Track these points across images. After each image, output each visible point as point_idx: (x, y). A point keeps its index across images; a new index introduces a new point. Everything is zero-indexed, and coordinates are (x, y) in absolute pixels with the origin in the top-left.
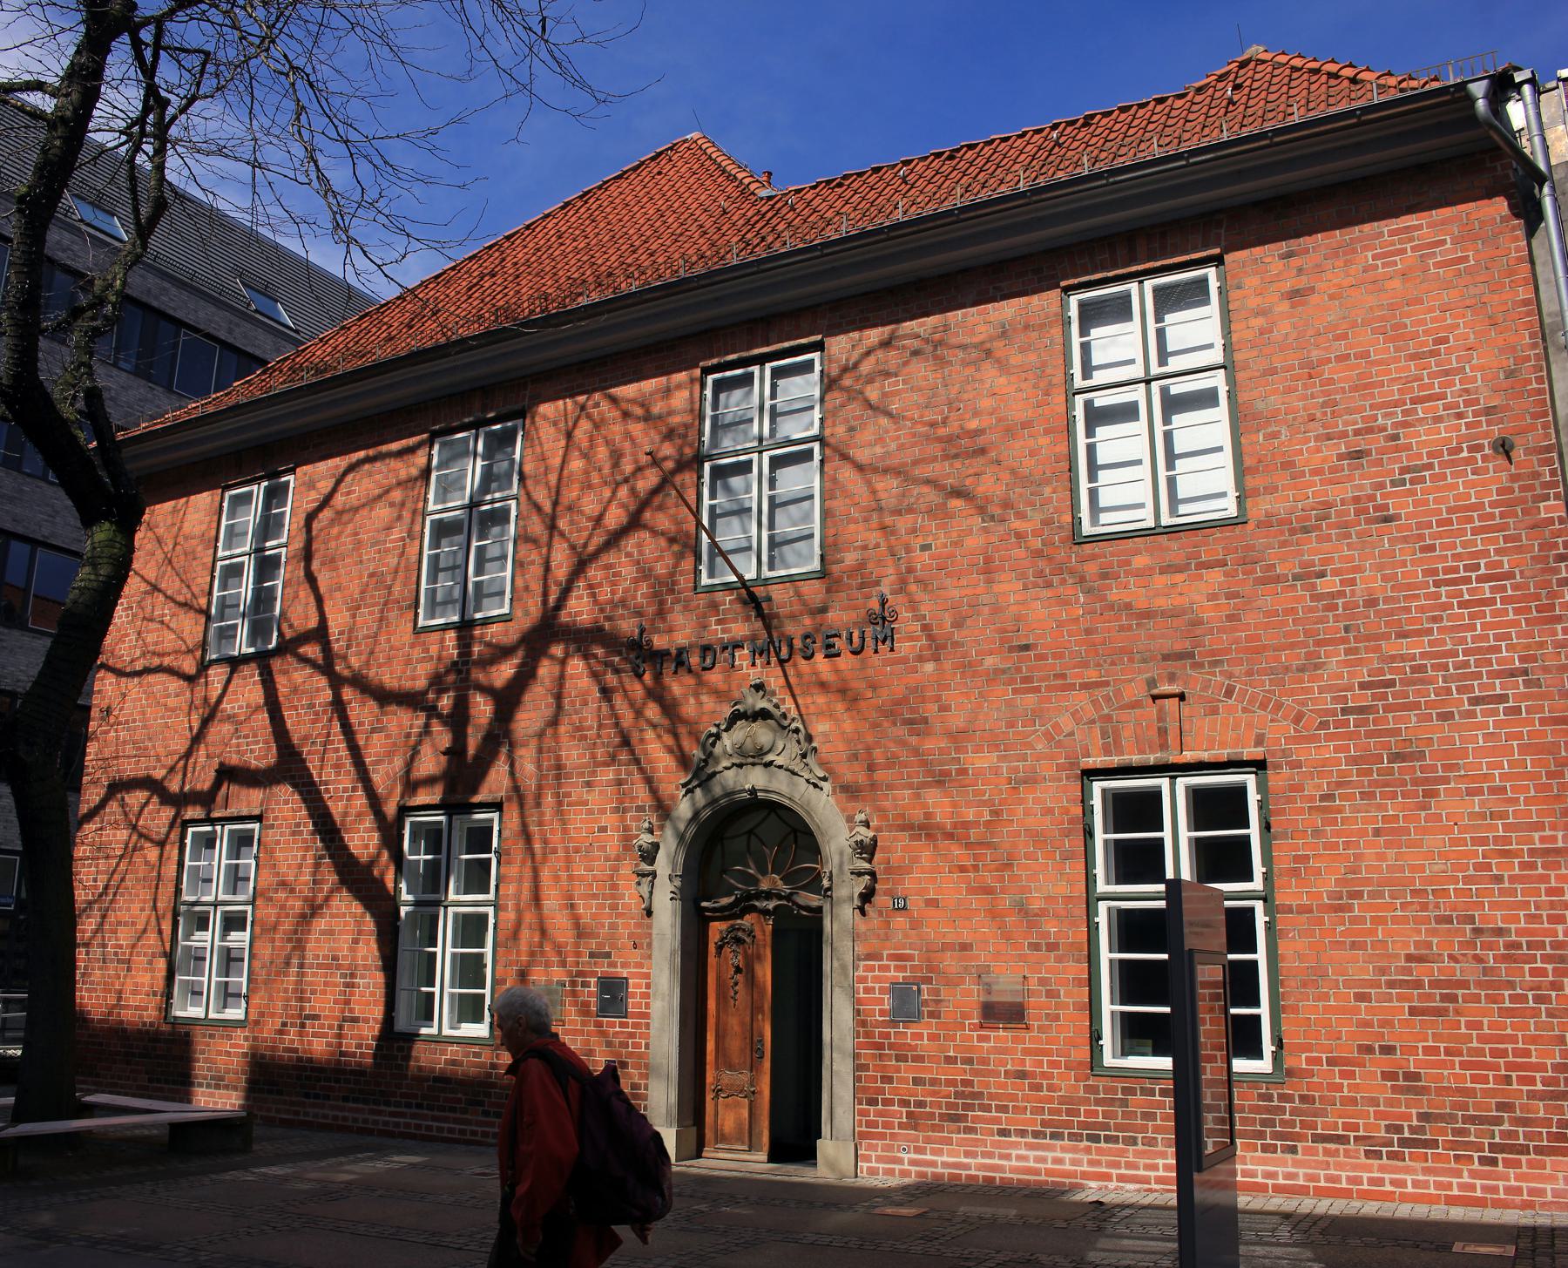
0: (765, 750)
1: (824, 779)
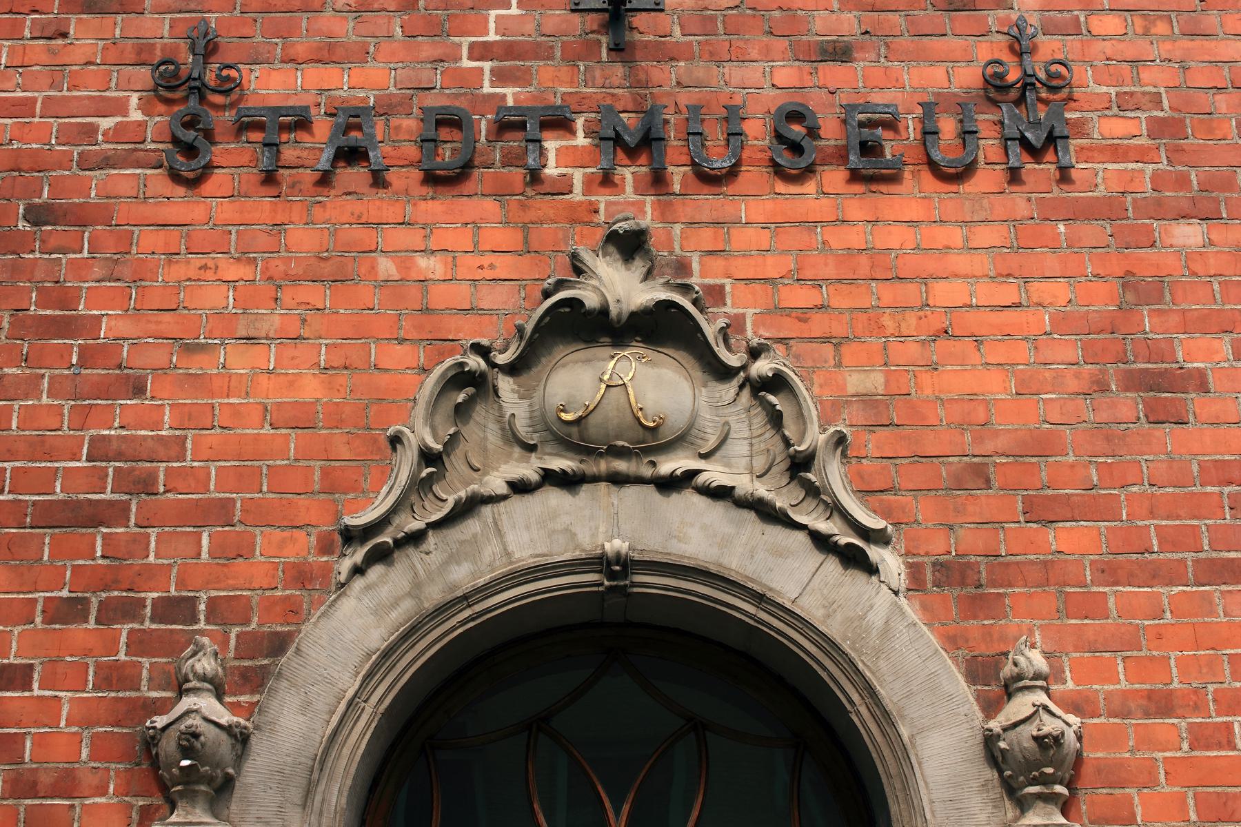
0: (667, 435)
1: (878, 537)
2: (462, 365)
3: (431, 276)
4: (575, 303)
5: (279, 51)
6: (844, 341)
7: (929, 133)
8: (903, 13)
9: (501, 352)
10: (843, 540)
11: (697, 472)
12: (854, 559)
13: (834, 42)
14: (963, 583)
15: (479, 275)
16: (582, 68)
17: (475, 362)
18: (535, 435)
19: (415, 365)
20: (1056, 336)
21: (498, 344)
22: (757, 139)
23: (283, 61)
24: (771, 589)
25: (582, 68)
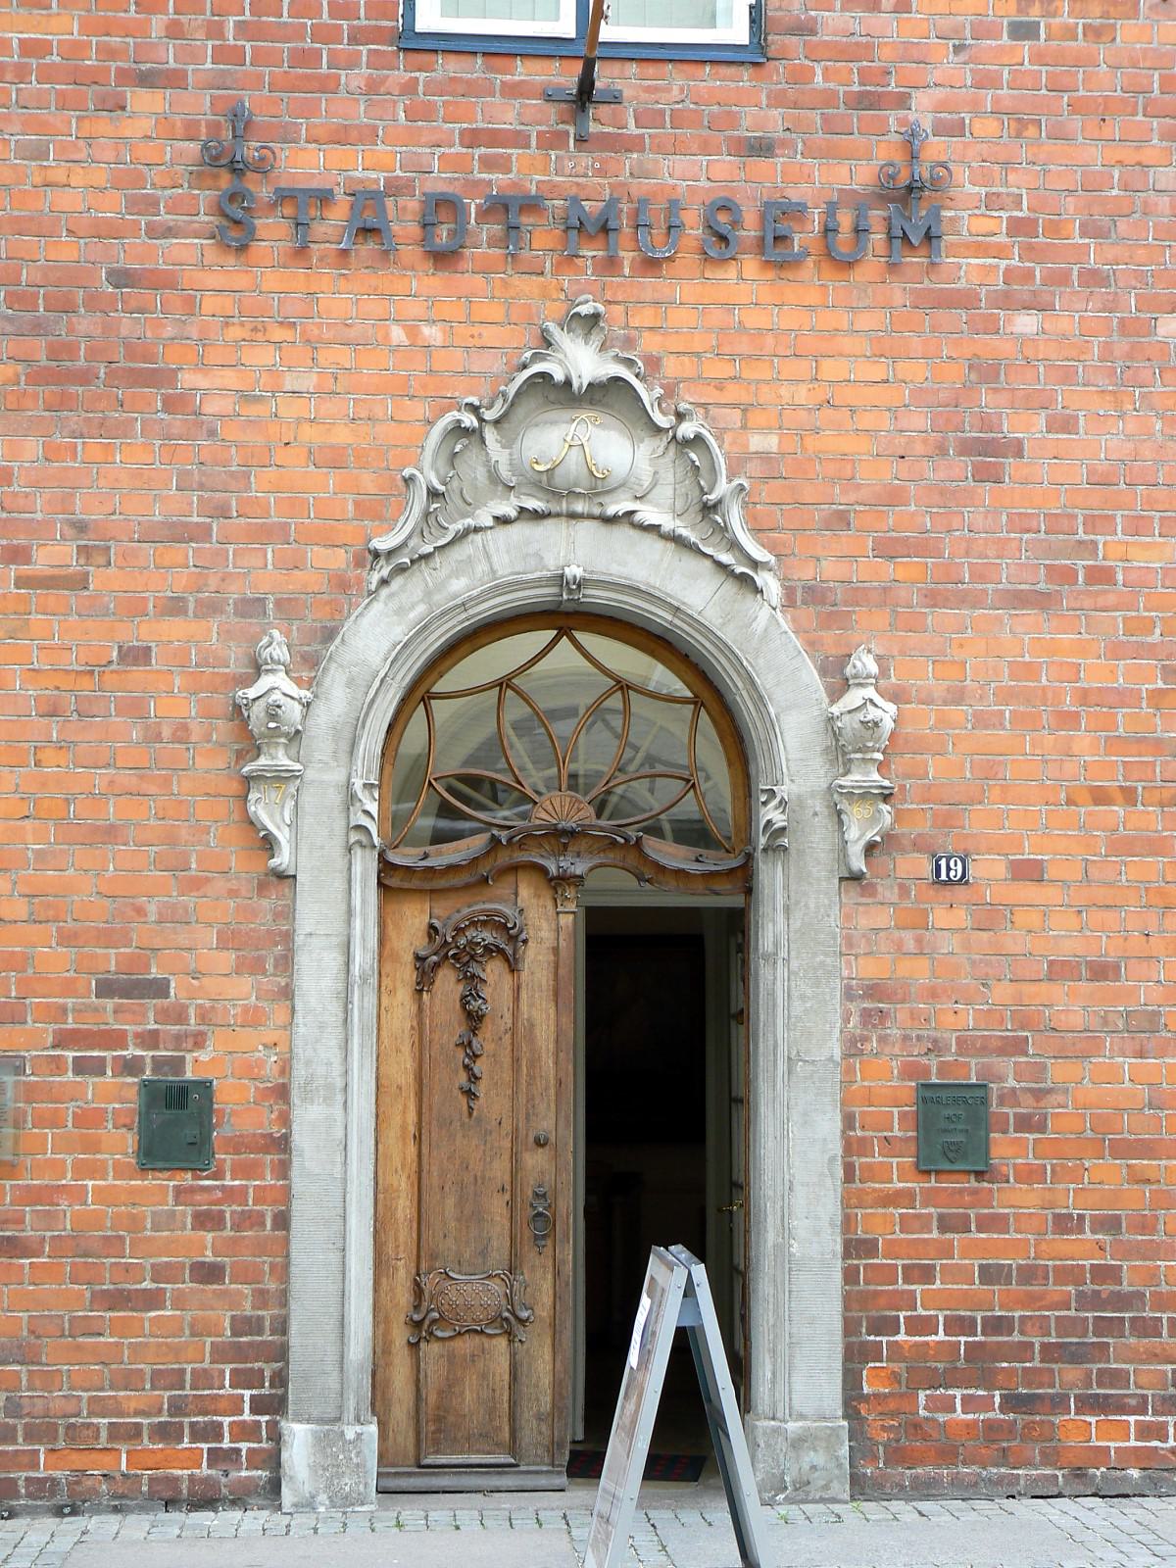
2: (459, 421)
3: (433, 343)
4: (545, 376)
5: (304, 131)
6: (750, 408)
7: (828, 231)
8: (819, 111)
9: (490, 407)
10: (739, 569)
11: (633, 512)
12: (745, 581)
13: (760, 138)
14: (823, 603)
15: (471, 342)
16: (553, 157)
17: (469, 420)
18: (514, 478)
19: (422, 418)
20: (912, 408)
21: (485, 402)
22: (692, 228)
23: (307, 142)
24: (684, 603)
25: (553, 157)
